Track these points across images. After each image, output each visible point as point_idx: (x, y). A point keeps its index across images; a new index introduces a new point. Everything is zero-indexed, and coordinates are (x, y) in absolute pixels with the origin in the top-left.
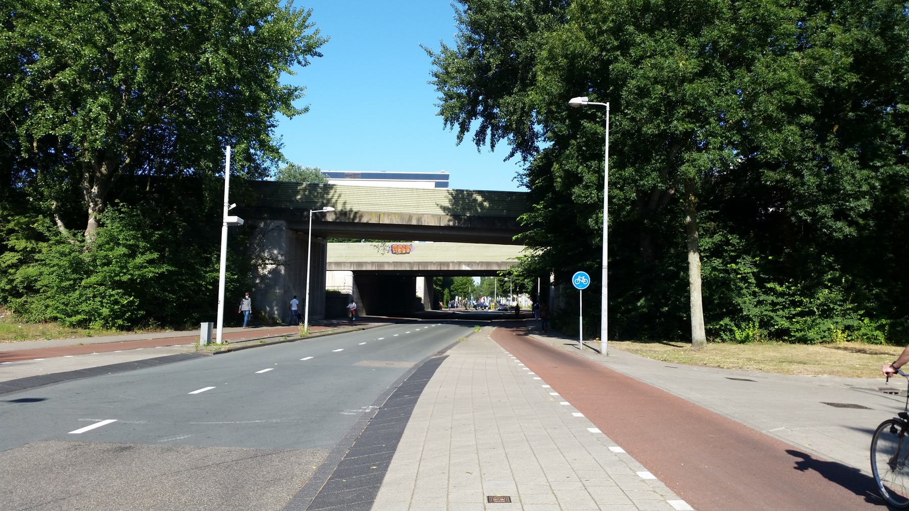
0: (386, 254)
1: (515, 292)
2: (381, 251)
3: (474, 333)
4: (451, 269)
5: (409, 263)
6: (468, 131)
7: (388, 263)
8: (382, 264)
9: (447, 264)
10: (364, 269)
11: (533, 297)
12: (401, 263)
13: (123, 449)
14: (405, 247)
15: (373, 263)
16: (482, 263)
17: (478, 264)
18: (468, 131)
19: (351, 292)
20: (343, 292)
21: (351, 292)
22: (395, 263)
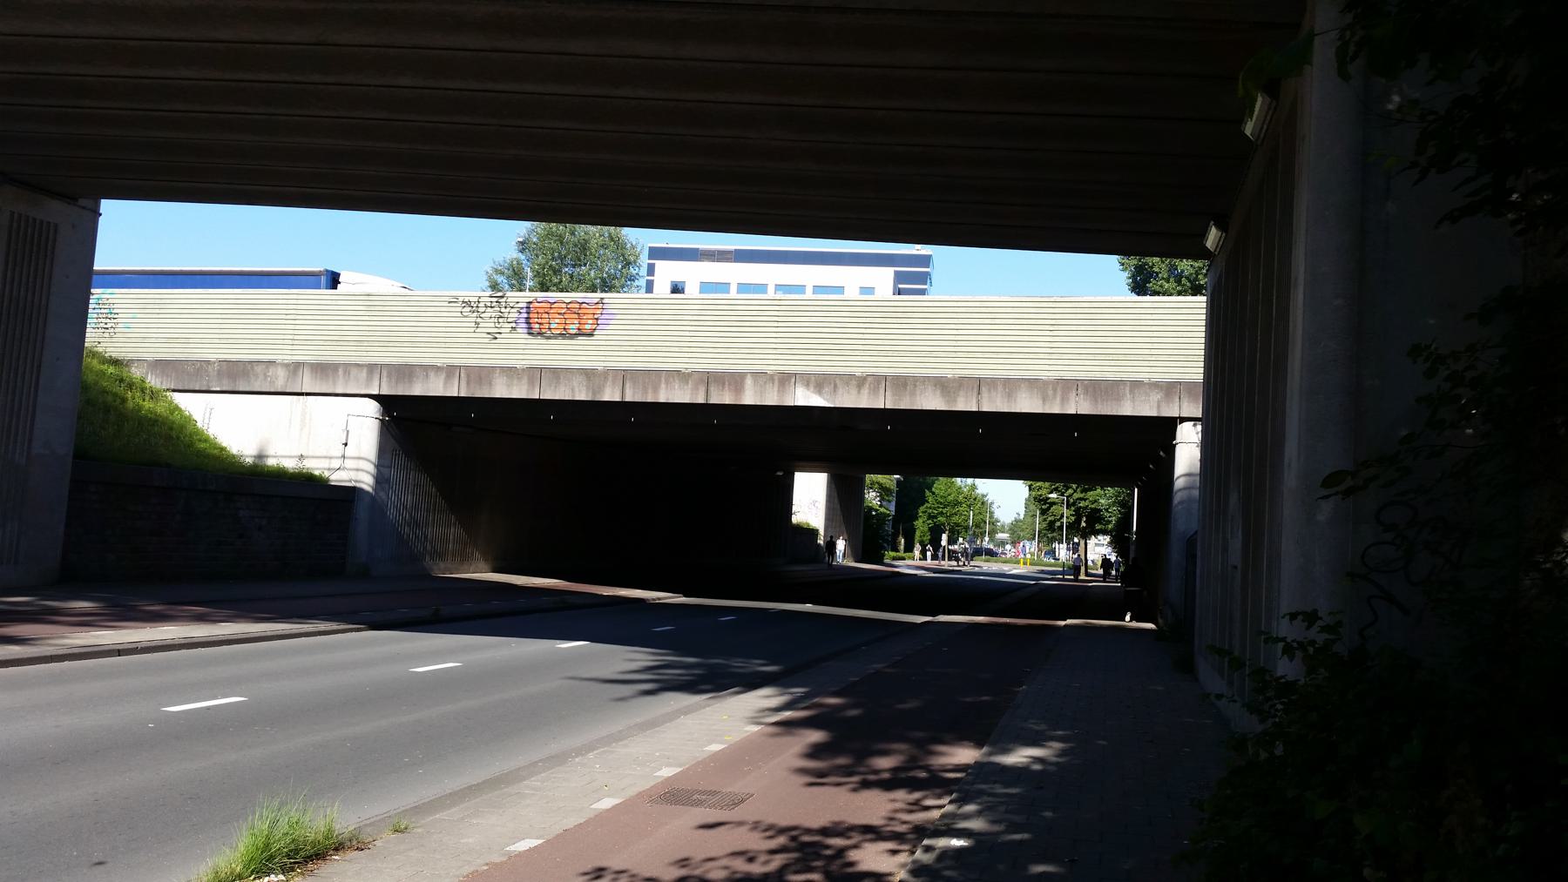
0: (506, 336)
1: (1074, 528)
2: (489, 326)
3: (687, 711)
4: (749, 399)
5: (588, 374)
6: (1141, 285)
7: (510, 372)
8: (481, 373)
9: (735, 380)
10: (417, 390)
11: (1118, 543)
12: (557, 373)
13: (100, 863)
14: (577, 311)
15: (450, 371)
16: (879, 381)
17: (861, 381)
18: (1141, 285)
19: (366, 481)
20: (339, 478)
21: (366, 481)
22: (536, 373)
